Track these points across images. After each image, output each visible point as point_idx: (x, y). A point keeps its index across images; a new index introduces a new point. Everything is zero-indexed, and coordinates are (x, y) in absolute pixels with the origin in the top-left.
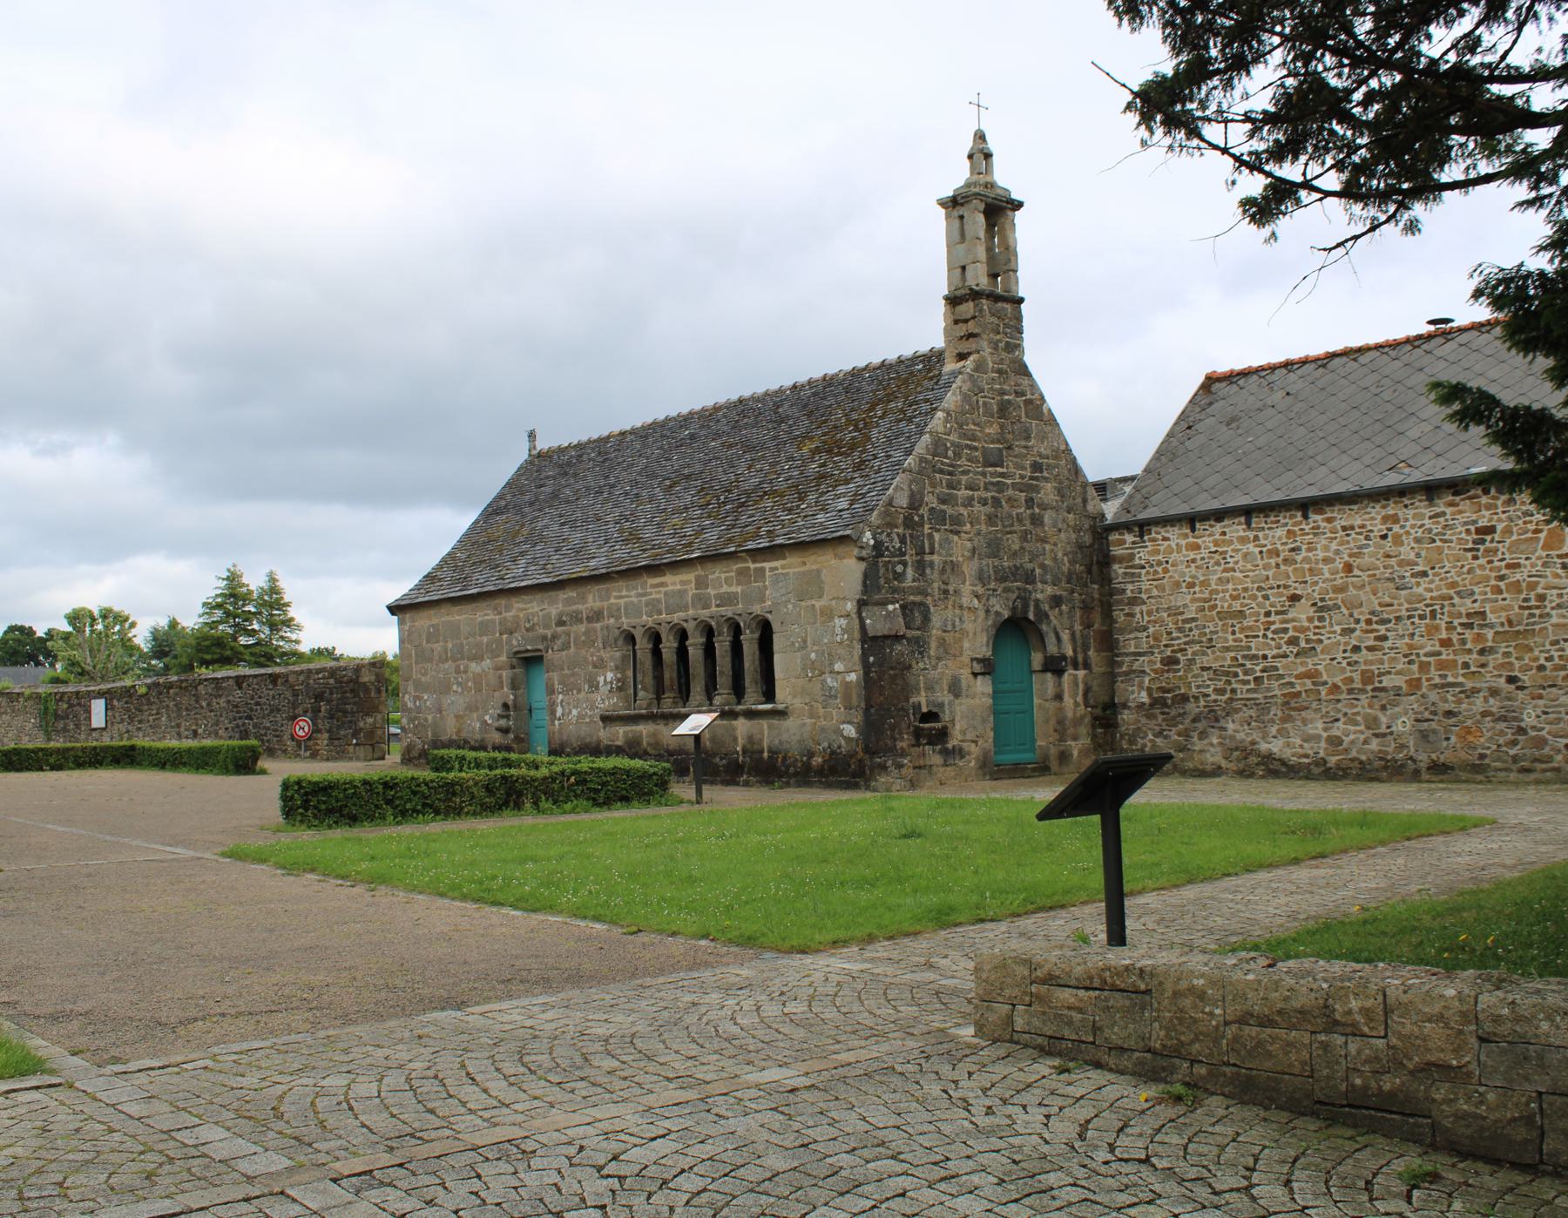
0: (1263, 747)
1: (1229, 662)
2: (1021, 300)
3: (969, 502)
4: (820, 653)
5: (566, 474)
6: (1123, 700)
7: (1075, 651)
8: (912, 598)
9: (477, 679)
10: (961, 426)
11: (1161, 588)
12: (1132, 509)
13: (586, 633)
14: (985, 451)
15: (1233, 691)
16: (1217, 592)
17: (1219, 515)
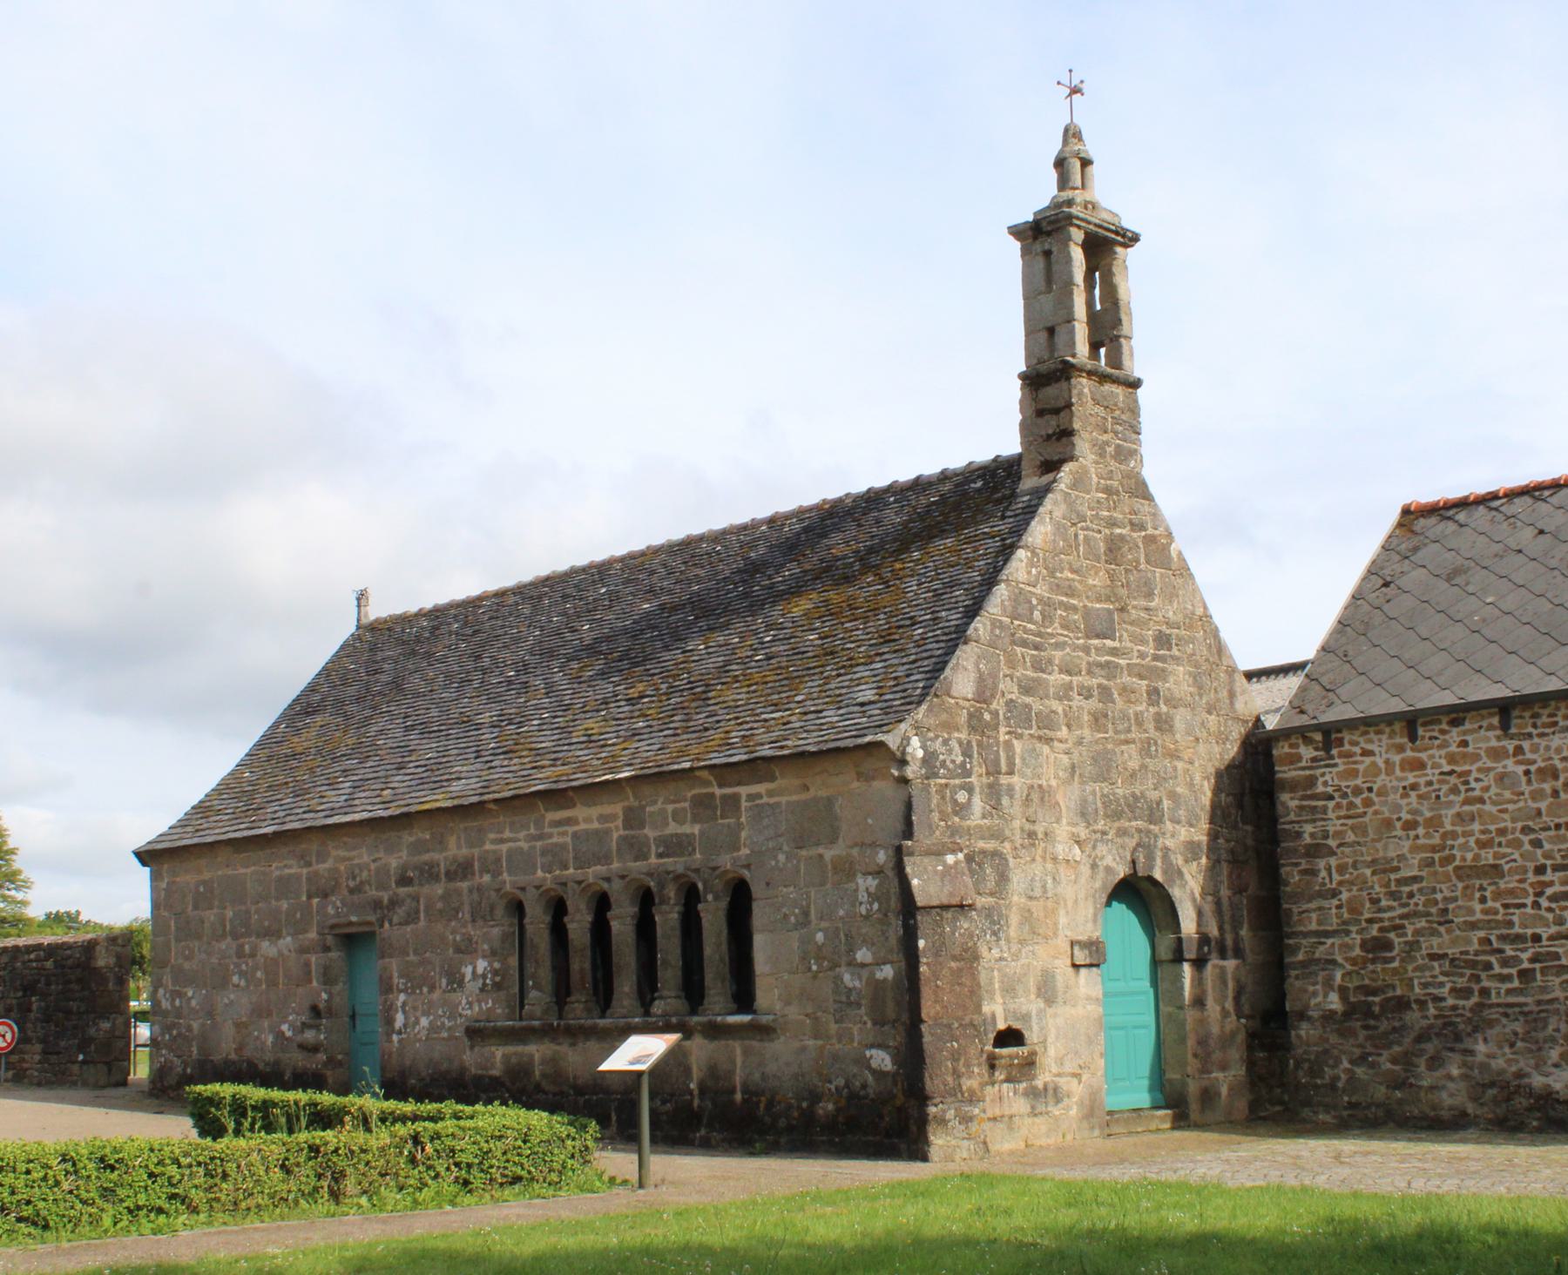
0: (1537, 1081)
1: (1476, 946)
2: (1135, 384)
3: (1065, 693)
4: (833, 935)
5: (414, 653)
6: (1298, 1006)
7: (1221, 928)
8: (981, 844)
9: (272, 966)
10: (1052, 574)
11: (1361, 830)
12: (1309, 707)
13: (445, 897)
14: (1087, 613)
15: (1485, 992)
16: (1454, 835)
17: (1457, 714)
